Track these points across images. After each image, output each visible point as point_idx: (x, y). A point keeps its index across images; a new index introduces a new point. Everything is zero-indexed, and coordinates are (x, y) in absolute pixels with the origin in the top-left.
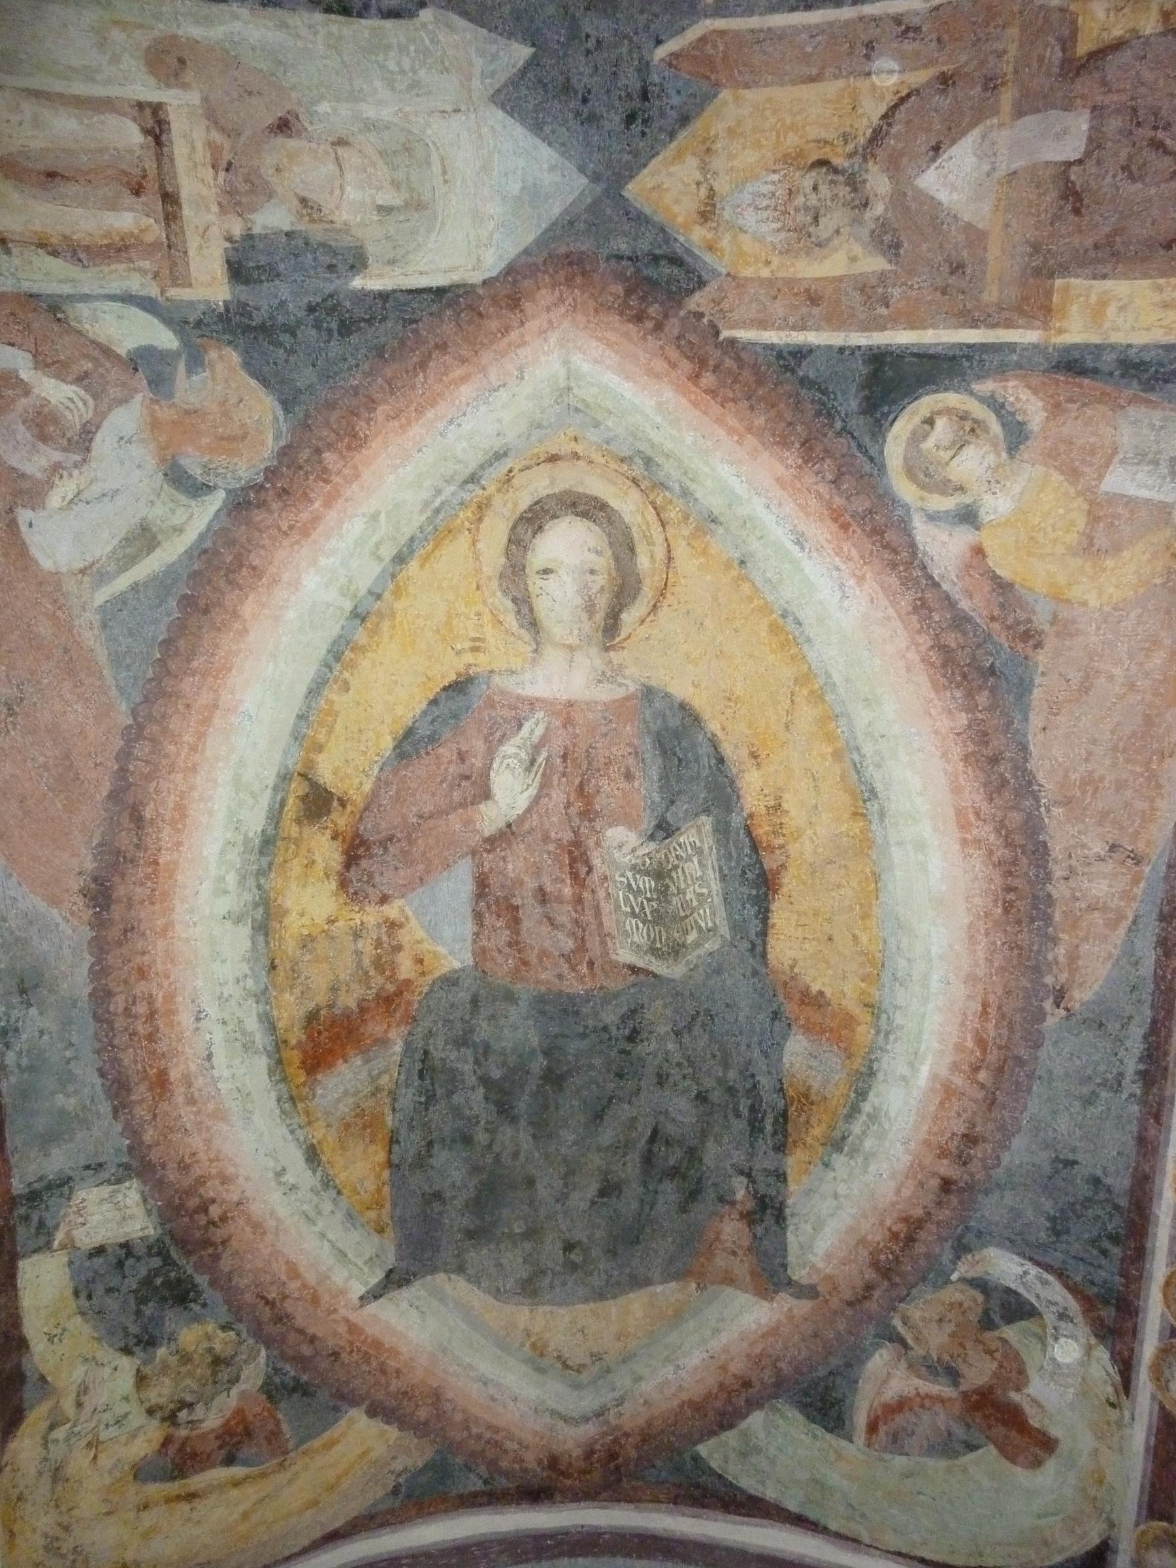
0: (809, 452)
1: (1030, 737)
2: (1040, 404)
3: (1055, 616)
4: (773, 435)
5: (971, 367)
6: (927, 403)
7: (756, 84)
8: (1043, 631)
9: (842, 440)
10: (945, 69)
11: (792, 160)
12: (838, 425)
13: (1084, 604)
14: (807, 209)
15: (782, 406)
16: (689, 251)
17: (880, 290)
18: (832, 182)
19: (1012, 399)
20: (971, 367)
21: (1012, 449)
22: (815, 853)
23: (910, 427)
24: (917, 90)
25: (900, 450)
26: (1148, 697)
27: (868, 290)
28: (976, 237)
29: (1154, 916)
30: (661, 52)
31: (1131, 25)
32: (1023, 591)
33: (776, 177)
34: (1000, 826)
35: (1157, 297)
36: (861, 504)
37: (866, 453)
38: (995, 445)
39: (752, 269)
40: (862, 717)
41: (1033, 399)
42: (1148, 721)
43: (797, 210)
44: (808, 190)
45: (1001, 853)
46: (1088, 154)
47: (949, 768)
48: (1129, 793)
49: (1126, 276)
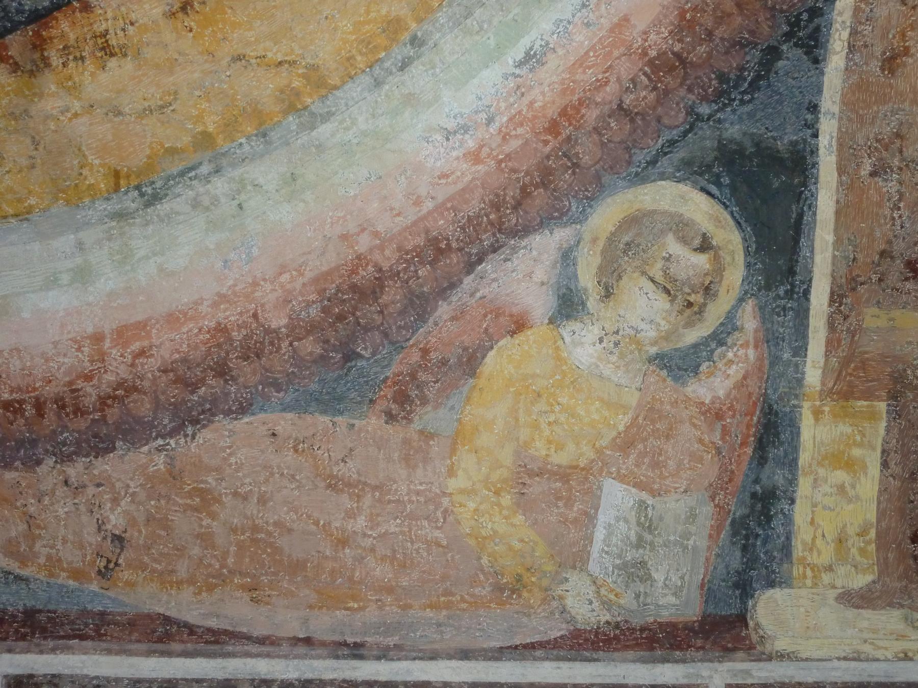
0: (665, 67)
1: (262, 416)
2: (721, 393)
3: (431, 436)
4: (695, 9)
5: (778, 297)
6: (731, 239)
8: (410, 421)
9: (682, 115)
12: (705, 110)
13: (451, 472)
19: (730, 355)
20: (778, 297)
21: (662, 361)
22: (47, 117)
25: (665, 205)
26: (329, 565)
27: (898, 142)
29: (30, 603)
32: (465, 389)
34: (128, 388)
35: (851, 531)
36: (587, 151)
38: (667, 338)
40: (267, 173)
41: (729, 383)
42: (297, 567)
45: (90, 393)
47: (204, 308)
48: (196, 551)
49: (883, 490)
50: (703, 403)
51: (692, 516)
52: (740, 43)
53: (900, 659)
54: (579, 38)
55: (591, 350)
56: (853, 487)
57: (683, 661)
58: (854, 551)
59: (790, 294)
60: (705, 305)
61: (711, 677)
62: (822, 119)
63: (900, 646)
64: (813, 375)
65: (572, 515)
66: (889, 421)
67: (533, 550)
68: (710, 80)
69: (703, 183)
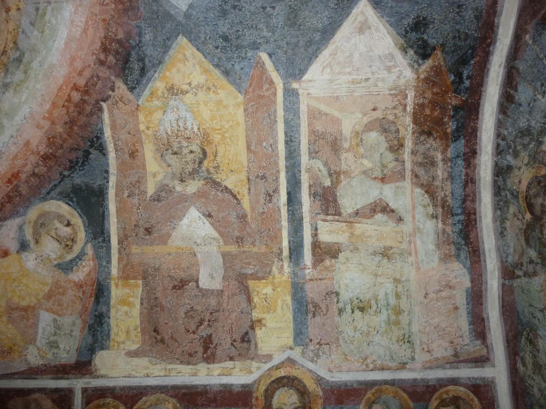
2: (82, 278)
5: (99, 242)
6: (78, 221)
7: (246, 116)
10: (249, 217)
11: (206, 139)
12: (66, 173)
14: (181, 148)
15: (71, 141)
16: (149, 80)
17: (137, 192)
18: (195, 161)
19: (84, 264)
23: (65, 214)
24: (240, 203)
25: (53, 209)
27: (138, 184)
28: (164, 240)
30: (264, 57)
31: (258, 306)
33: (196, 130)
37: (52, 189)
38: (60, 258)
39: (143, 119)
41: (84, 274)
43: (179, 142)
44: (190, 148)
46: (201, 290)
49: (141, 313)
50: (75, 282)
51: (74, 324)
52: (73, 149)
53: (145, 377)
54: (13, 148)
55: (33, 263)
56: (131, 312)
57: (67, 379)
58: (133, 336)
59: (104, 241)
60: (72, 246)
61: (76, 385)
62: (110, 176)
63: (146, 372)
64: (114, 271)
65: (29, 324)
66: (143, 288)
67: (16, 337)
68: (67, 162)
69: (67, 201)
